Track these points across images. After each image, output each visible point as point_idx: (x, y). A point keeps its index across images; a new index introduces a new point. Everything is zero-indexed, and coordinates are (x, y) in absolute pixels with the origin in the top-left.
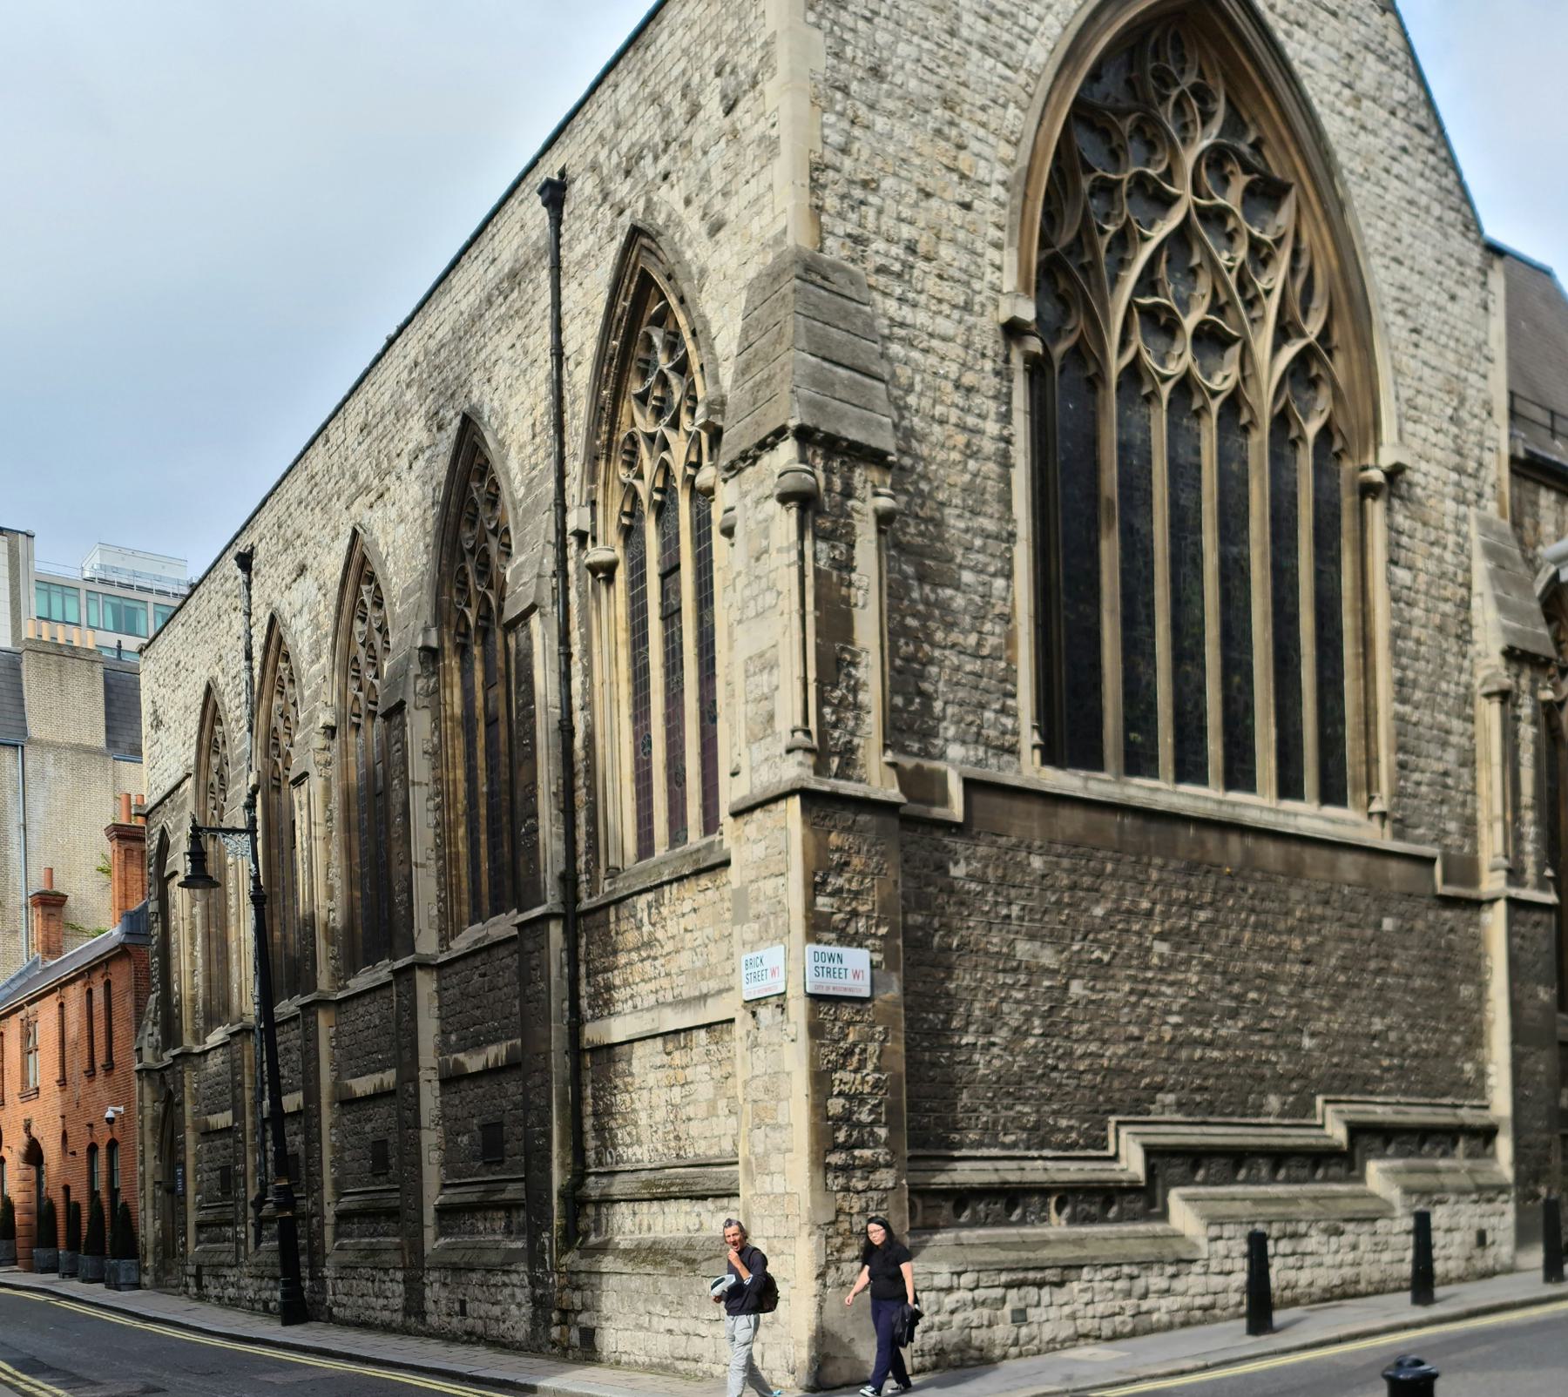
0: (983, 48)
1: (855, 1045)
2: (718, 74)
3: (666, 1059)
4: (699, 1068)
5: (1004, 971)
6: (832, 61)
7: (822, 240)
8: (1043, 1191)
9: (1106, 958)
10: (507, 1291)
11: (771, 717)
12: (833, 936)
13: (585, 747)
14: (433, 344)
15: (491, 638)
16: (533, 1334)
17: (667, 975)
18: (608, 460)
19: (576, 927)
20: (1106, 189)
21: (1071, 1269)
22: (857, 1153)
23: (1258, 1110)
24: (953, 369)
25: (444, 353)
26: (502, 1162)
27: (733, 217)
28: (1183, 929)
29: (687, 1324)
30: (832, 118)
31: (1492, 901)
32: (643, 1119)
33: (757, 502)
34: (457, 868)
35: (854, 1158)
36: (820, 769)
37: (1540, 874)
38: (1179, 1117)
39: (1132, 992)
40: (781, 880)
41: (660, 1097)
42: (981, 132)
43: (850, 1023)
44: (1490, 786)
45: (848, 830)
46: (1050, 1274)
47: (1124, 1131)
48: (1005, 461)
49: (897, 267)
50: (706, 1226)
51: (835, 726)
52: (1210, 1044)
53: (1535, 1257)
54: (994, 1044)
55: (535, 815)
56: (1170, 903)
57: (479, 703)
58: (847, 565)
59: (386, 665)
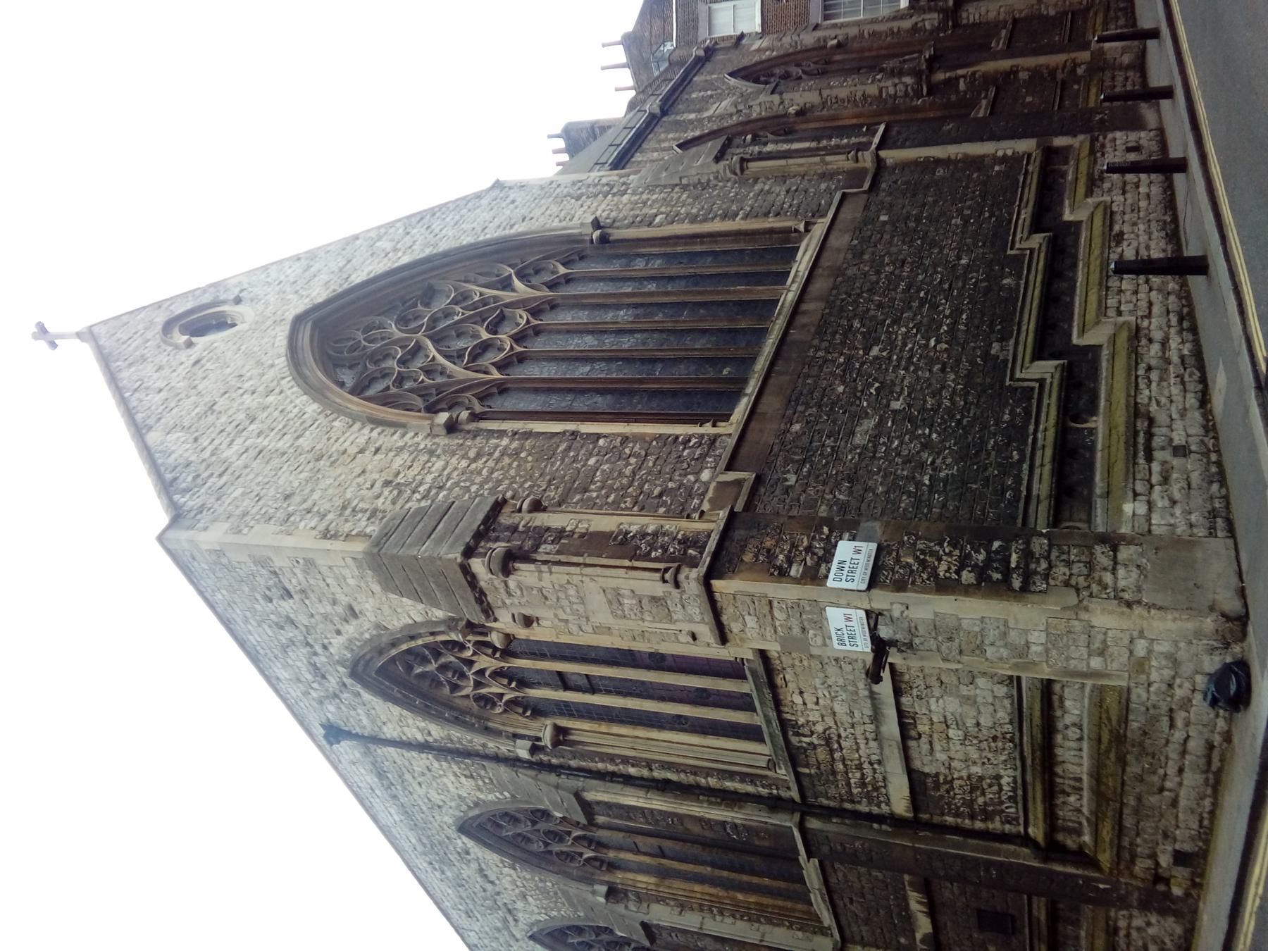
0: (298, 438)
1: (916, 558)
2: (271, 601)
3: (924, 739)
4: (933, 707)
5: (875, 452)
6: (272, 522)
7: (366, 535)
8: (1063, 432)
9: (877, 385)
10: (1134, 934)
11: (654, 599)
12: (823, 566)
13: (678, 772)
14: (420, 848)
15: (604, 840)
16: (1178, 915)
17: (853, 726)
18: (488, 720)
19: (813, 806)
20: (400, 380)
21: (1136, 411)
22: (1013, 565)
23: (1013, 290)
24: (464, 463)
25: (425, 841)
26: (1013, 917)
27: (347, 599)
28: (864, 337)
29: (1172, 751)
30: (302, 524)
31: (879, 161)
32: (976, 770)
33: (509, 594)
34: (767, 906)
35: (1017, 567)
36: (694, 564)
37: (864, 135)
38: (1012, 341)
39: (906, 369)
40: (775, 604)
41: (957, 750)
42: (341, 440)
43: (898, 560)
44: (802, 165)
45: (743, 549)
46: (1142, 425)
47: (1018, 375)
48: (529, 435)
49: (395, 492)
50: (1076, 719)
51: (665, 550)
52: (955, 322)
53: (1147, 112)
54: (933, 462)
55: (723, 824)
56: (843, 343)
57: (647, 859)
58: (561, 533)
59: (620, 934)
